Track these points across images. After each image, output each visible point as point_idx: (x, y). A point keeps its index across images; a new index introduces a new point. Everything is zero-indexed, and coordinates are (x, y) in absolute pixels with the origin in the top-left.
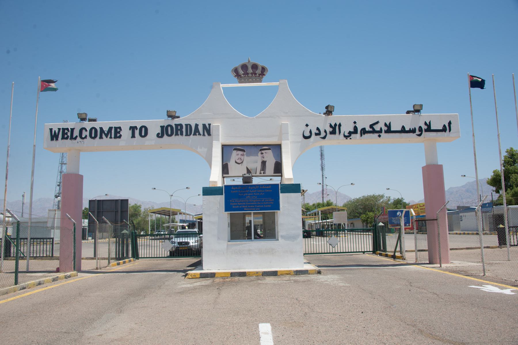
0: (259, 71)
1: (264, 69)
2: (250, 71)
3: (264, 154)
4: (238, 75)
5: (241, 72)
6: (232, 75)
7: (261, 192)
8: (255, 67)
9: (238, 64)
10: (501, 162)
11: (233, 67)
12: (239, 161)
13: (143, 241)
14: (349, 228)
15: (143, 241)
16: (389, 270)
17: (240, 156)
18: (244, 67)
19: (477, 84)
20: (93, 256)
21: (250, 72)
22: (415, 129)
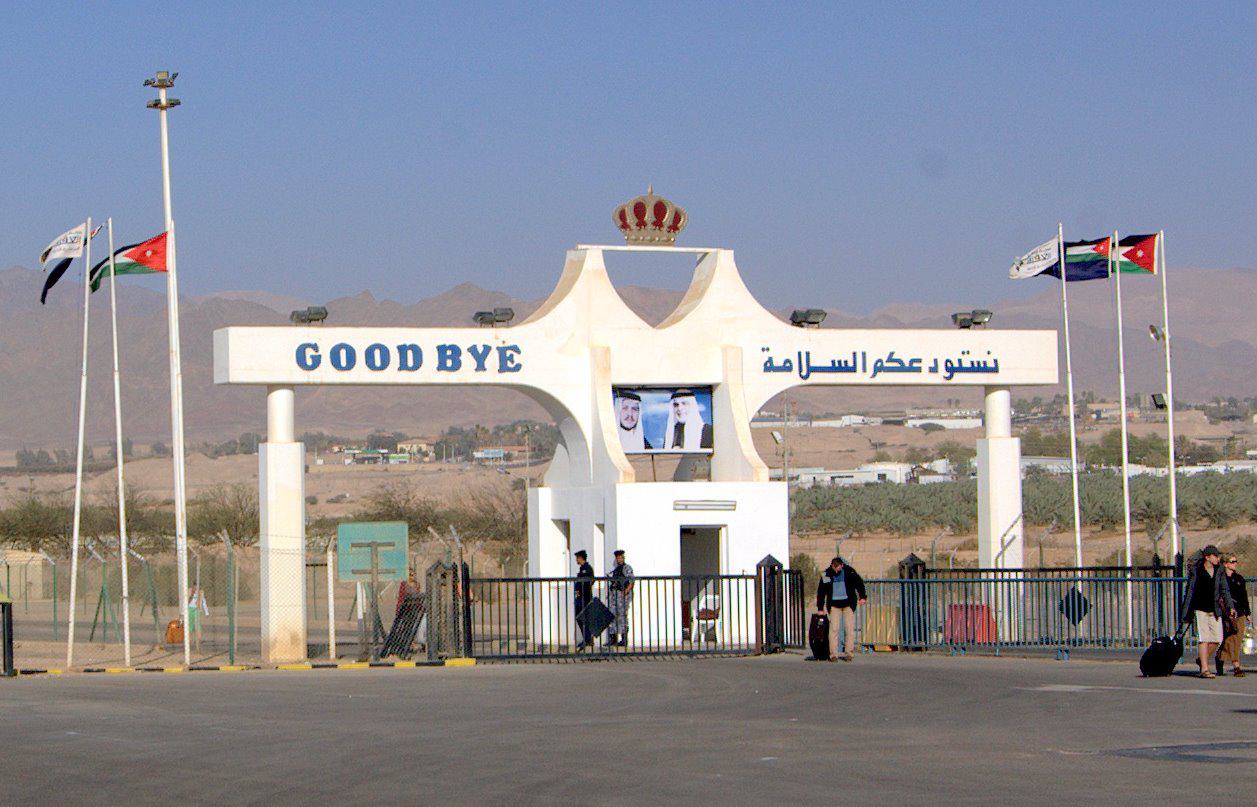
0: (668, 219)
2: (649, 217)
3: (681, 407)
5: (631, 219)
17: (629, 412)
21: (652, 216)
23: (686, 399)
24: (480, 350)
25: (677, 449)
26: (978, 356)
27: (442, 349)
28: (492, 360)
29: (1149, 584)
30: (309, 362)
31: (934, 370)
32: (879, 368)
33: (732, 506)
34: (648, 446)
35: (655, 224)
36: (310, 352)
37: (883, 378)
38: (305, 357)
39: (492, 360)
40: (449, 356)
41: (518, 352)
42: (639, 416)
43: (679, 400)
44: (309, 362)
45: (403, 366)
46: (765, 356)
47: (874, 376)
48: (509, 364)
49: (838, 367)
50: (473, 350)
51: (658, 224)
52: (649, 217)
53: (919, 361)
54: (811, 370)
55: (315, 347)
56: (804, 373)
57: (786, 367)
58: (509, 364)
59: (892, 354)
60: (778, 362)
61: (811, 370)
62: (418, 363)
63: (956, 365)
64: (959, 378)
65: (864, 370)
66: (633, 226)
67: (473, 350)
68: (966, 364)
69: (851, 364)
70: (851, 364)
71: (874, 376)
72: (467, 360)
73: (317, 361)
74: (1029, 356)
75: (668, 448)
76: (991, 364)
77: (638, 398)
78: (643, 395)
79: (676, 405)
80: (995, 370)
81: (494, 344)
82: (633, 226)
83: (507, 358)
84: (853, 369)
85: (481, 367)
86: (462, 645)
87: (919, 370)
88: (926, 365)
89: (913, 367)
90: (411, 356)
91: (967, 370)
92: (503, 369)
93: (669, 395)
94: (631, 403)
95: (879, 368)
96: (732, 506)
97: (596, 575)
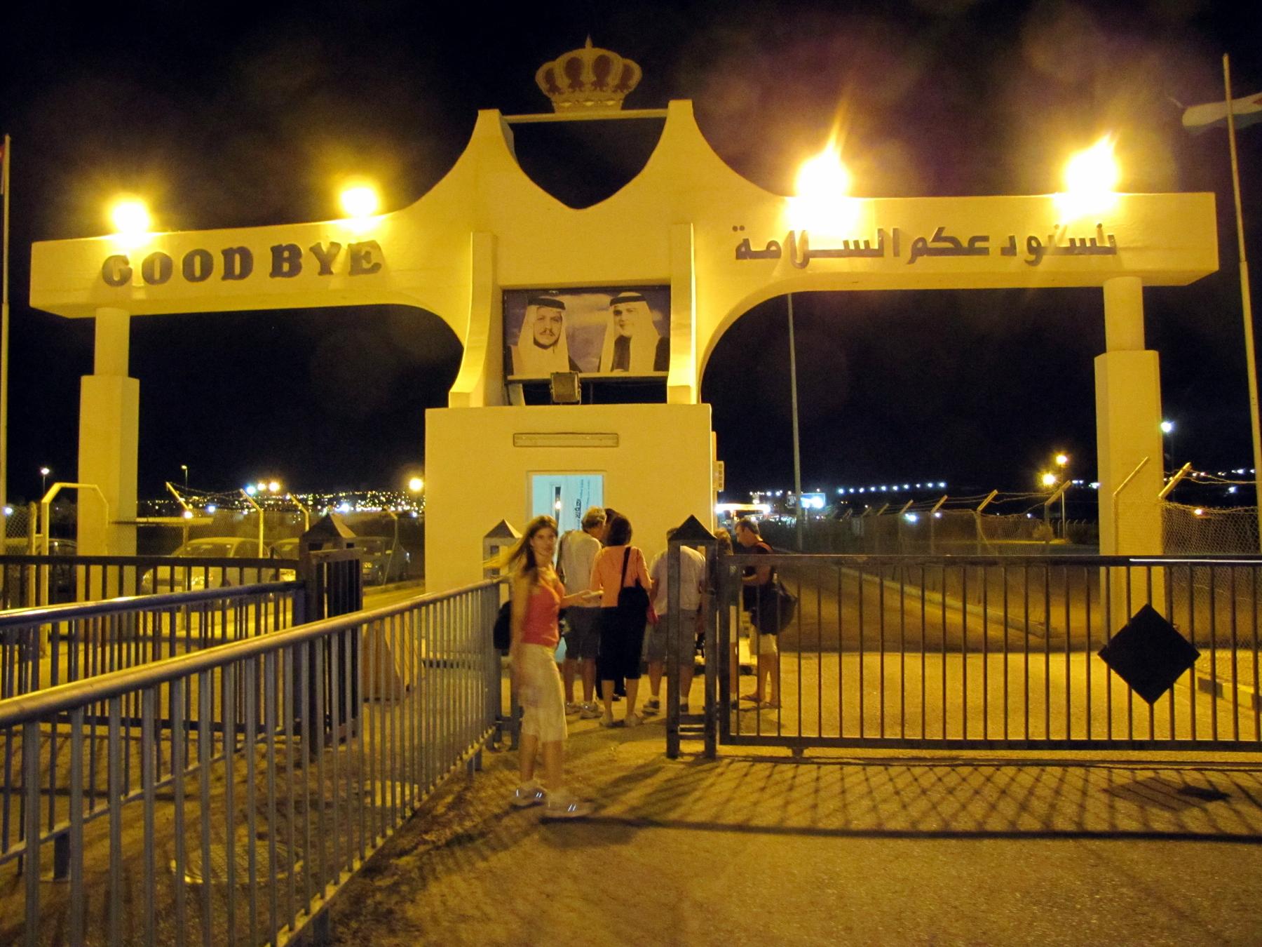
3: (625, 316)
12: (544, 340)
17: (548, 324)
19: (558, 490)
31: (1010, 250)
42: (562, 331)
77: (560, 305)
78: (566, 299)
79: (618, 313)
94: (550, 312)
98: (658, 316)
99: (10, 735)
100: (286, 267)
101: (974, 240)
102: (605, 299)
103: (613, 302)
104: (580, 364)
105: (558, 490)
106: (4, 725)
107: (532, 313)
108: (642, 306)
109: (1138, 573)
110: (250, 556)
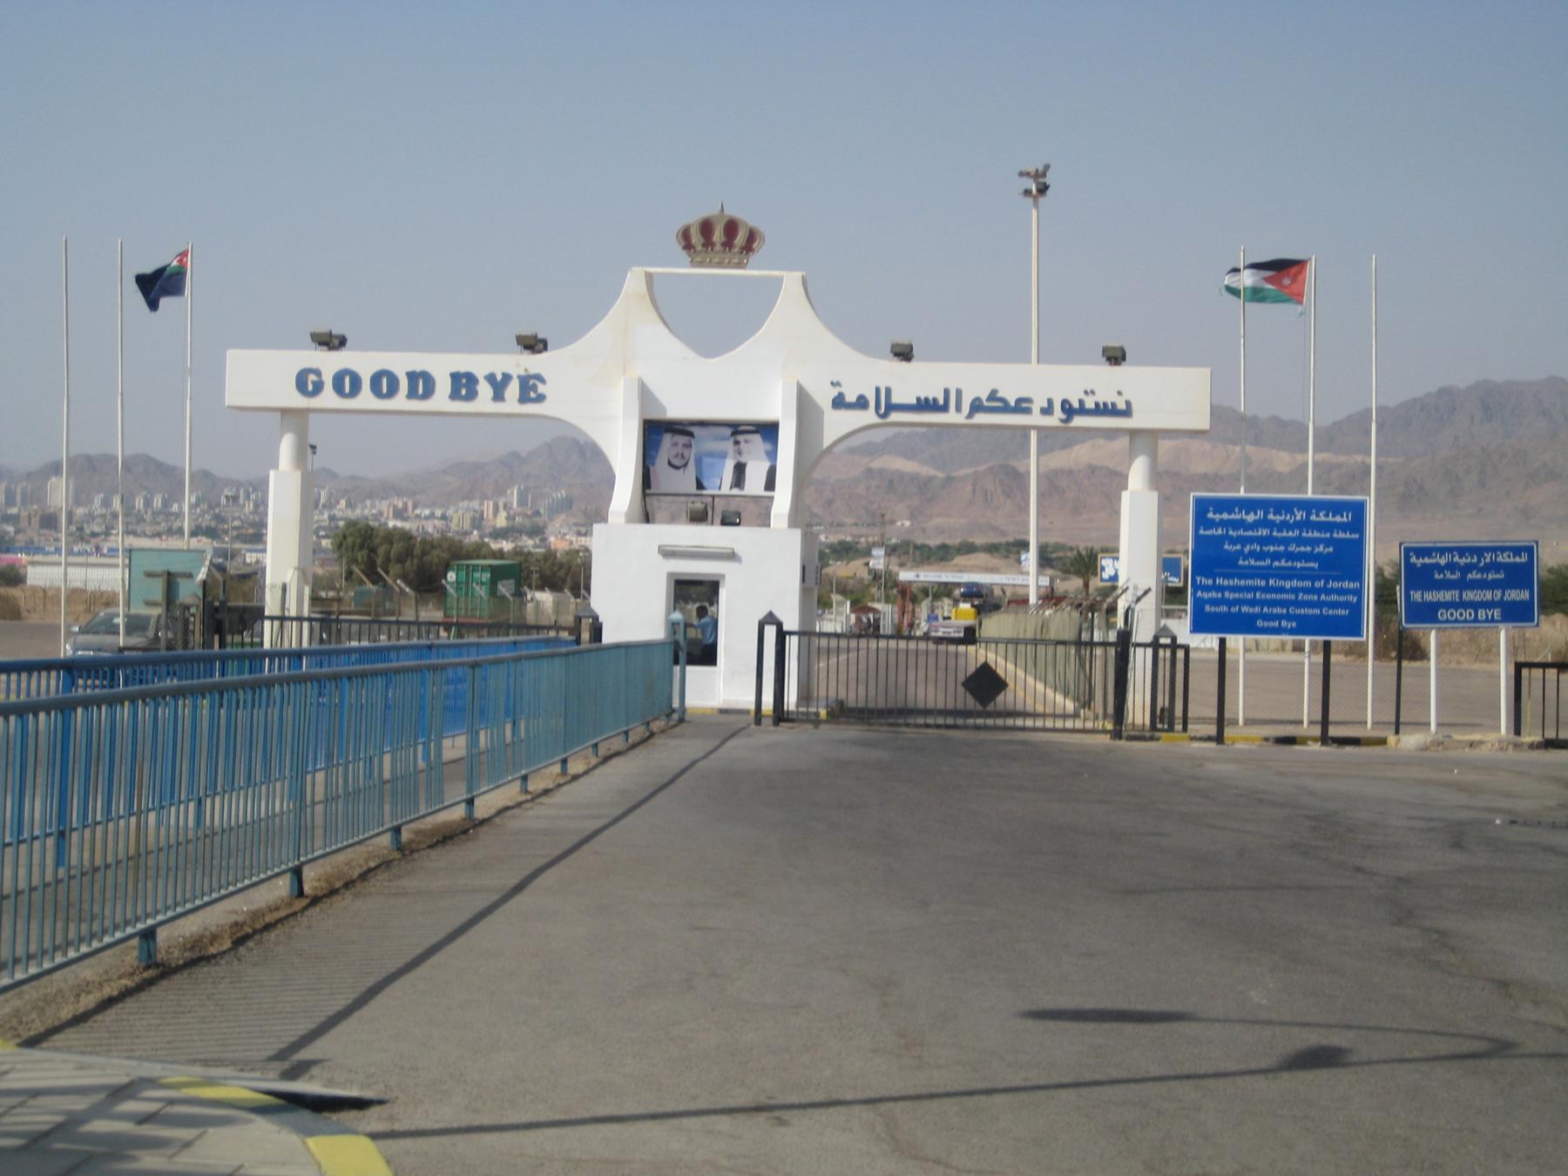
0: (740, 240)
1: (752, 236)
2: (718, 235)
3: (742, 445)
4: (688, 246)
5: (696, 239)
6: (676, 247)
7: (1317, 541)
8: (731, 227)
9: (693, 217)
10: (386, 489)
11: (678, 226)
12: (676, 462)
13: (44, 682)
14: (316, 646)
15: (44, 682)
16: (984, 735)
17: (679, 449)
18: (706, 227)
19: (157, 285)
20: (1525, 672)
21: (719, 238)
22: (541, 398)
23: (749, 437)
24: (499, 377)
25: (736, 491)
26: (1105, 396)
27: (456, 377)
28: (513, 390)
29: (306, 625)
30: (310, 387)
31: (1047, 411)
32: (977, 407)
33: (732, 556)
34: (700, 486)
35: (724, 244)
36: (312, 377)
37: (981, 418)
38: (306, 382)
39: (513, 390)
40: (463, 385)
41: (543, 381)
42: (692, 454)
43: (741, 438)
44: (310, 387)
45: (412, 394)
46: (834, 392)
47: (970, 416)
48: (533, 395)
49: (925, 405)
50: (491, 378)
51: (728, 244)
52: (718, 235)
53: (1029, 400)
54: (891, 407)
55: (318, 373)
56: (882, 411)
57: (861, 403)
58: (533, 395)
59: (994, 392)
60: (851, 398)
61: (891, 407)
62: (429, 392)
63: (1076, 405)
64: (1079, 421)
65: (958, 409)
66: (699, 248)
67: (491, 378)
68: (1090, 404)
69: (941, 402)
70: (941, 402)
71: (970, 416)
72: (485, 390)
73: (318, 387)
74: (1169, 396)
75: (726, 490)
76: (1122, 406)
77: (691, 435)
78: (695, 430)
79: (737, 443)
80: (1127, 413)
81: (515, 372)
82: (699, 248)
83: (530, 388)
84: (944, 408)
85: (498, 396)
86: (901, 721)
87: (1028, 411)
88: (1039, 403)
89: (1022, 406)
90: (421, 384)
91: (1089, 413)
92: (524, 399)
93: (729, 431)
94: (682, 439)
95: (977, 407)
96: (732, 556)
97: (267, 613)
98: (769, 447)
99: (7, 719)
100: (464, 392)
101: (1019, 401)
102: (729, 431)
103: (733, 434)
104: (705, 483)
105: (157, 285)
106: (4, 711)
107: (667, 440)
108: (757, 438)
109: (1099, 651)
110: (901, 705)
